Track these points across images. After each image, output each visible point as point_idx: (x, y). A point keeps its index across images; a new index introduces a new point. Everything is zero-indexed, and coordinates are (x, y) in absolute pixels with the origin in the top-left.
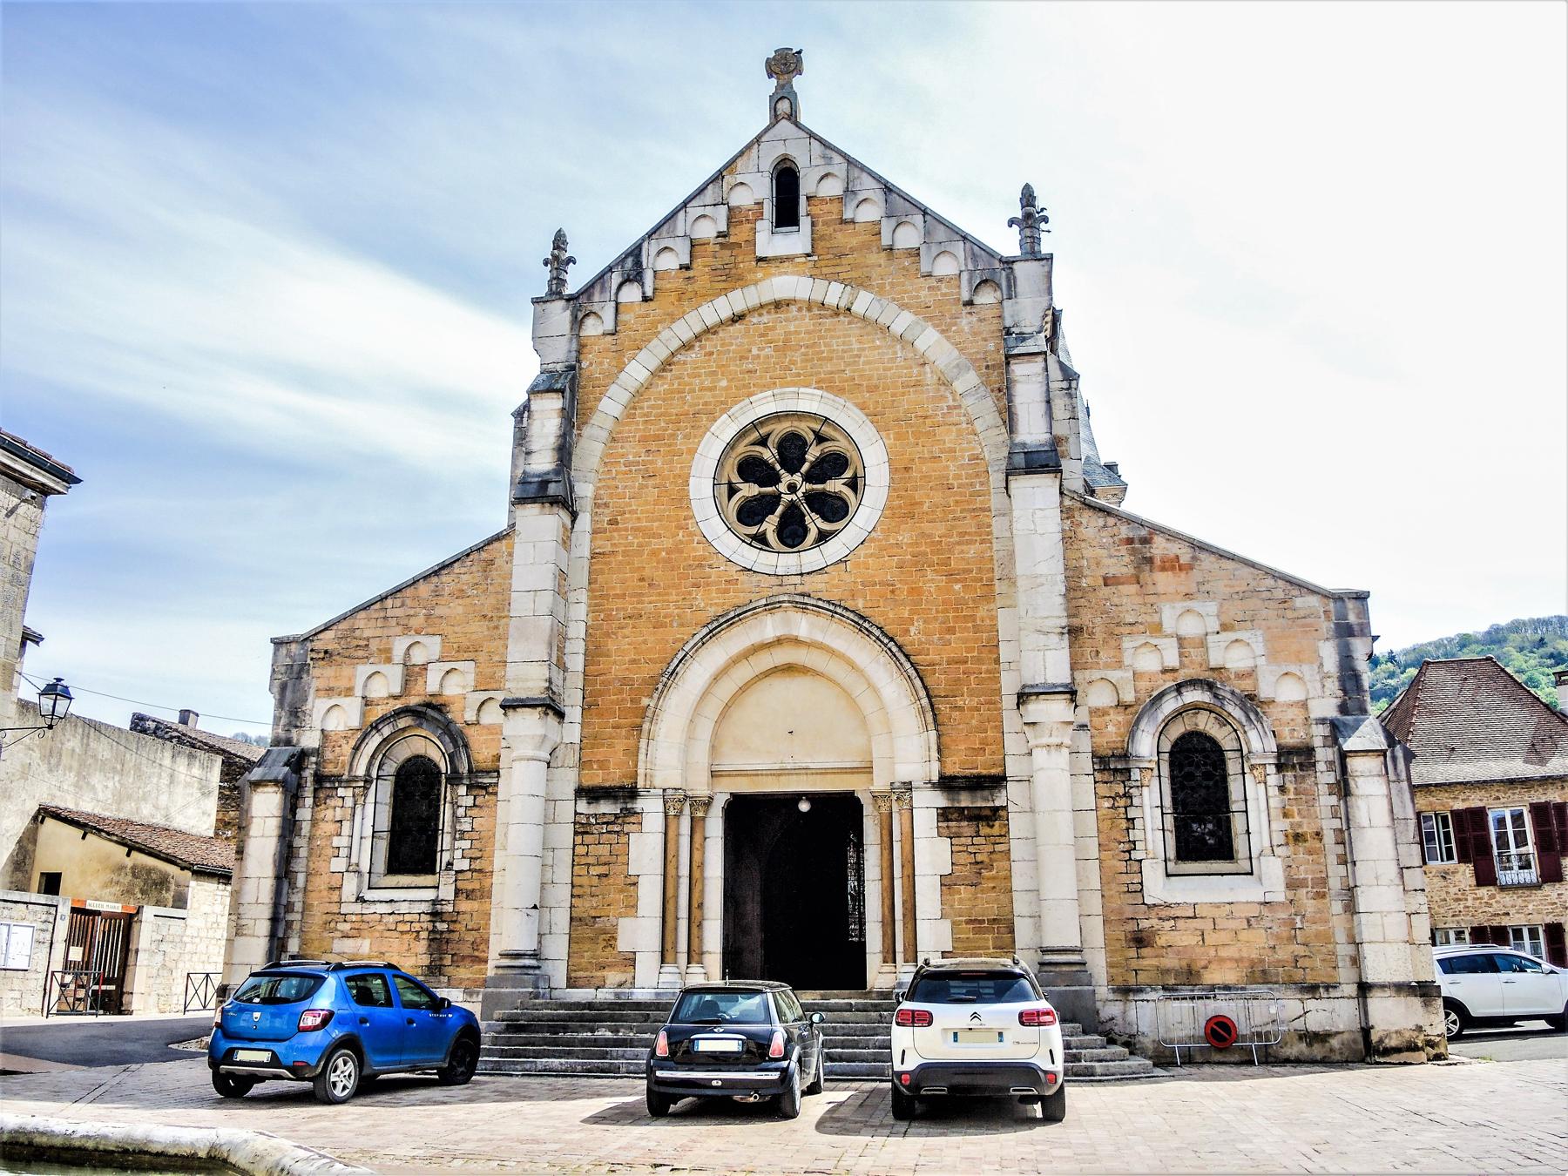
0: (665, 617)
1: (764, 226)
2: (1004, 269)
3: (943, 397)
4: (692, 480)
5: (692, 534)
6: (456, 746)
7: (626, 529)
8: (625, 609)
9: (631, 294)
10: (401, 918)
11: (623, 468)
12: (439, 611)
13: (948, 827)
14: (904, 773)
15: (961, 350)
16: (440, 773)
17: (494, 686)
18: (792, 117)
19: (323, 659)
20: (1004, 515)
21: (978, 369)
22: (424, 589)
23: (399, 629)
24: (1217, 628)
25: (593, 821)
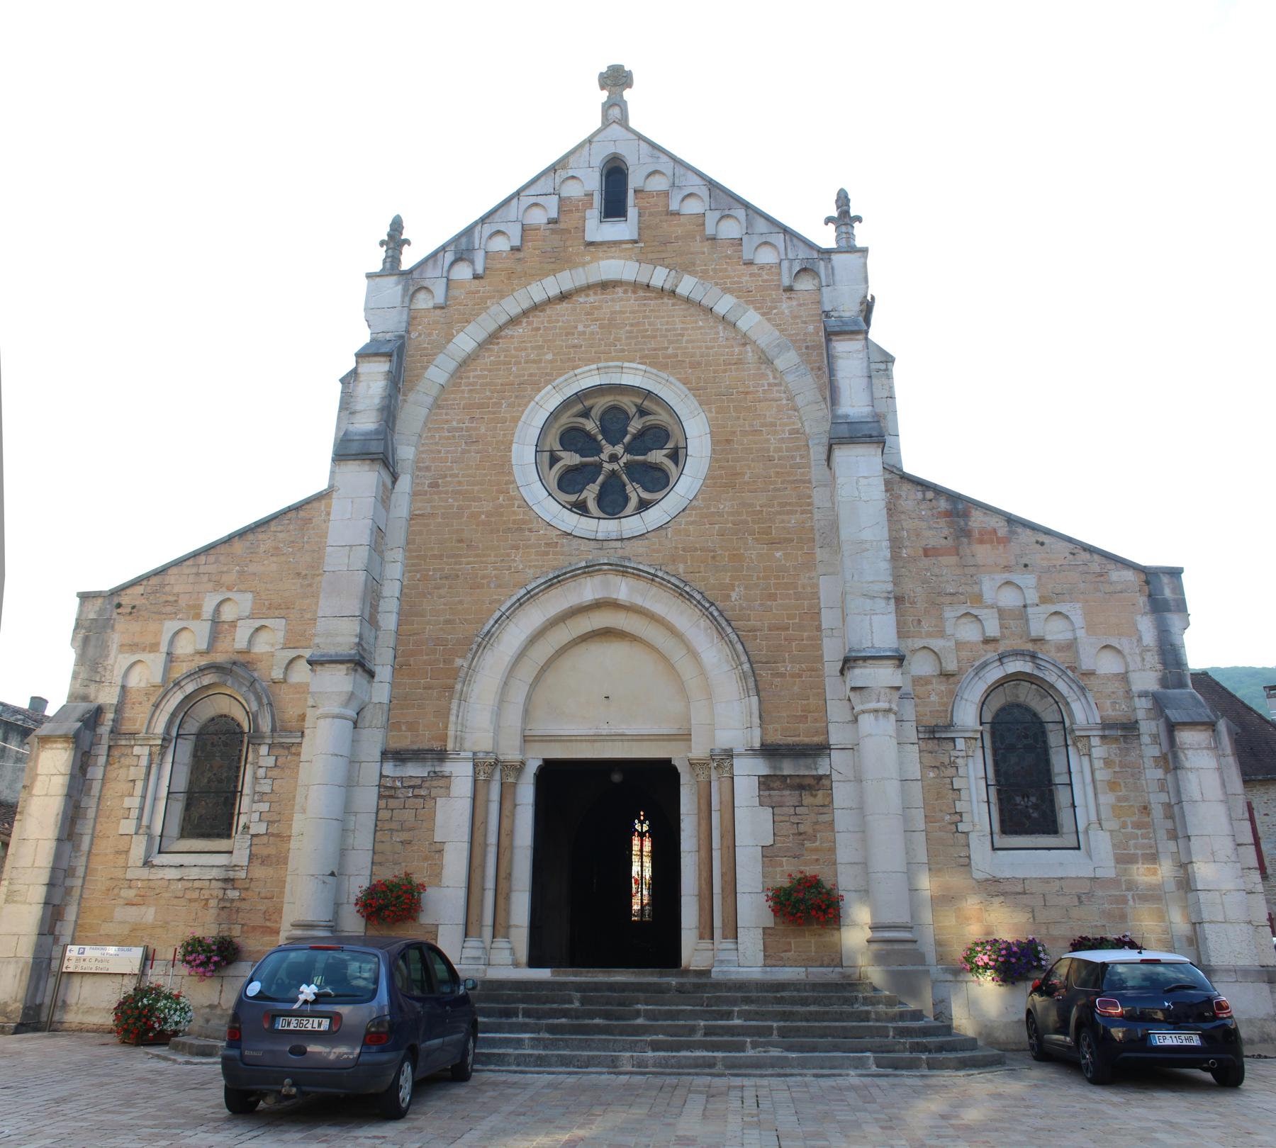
13: (770, 795)
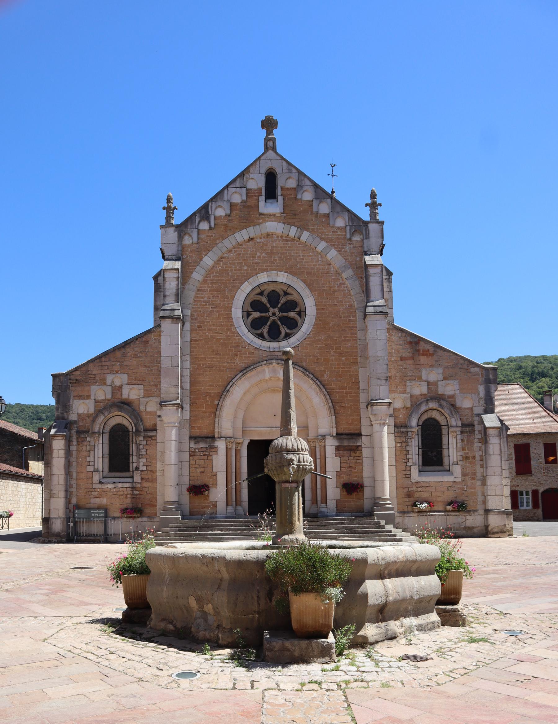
0: (223, 367)
1: (262, 198)
2: (364, 226)
3: (338, 279)
4: (233, 309)
5: (234, 333)
6: (137, 420)
7: (205, 330)
8: (206, 364)
9: (204, 226)
10: (119, 490)
11: (203, 303)
12: (125, 363)
14: (322, 431)
15: (346, 260)
16: (128, 431)
17: (152, 396)
18: (274, 149)
19: (76, 383)
20: (363, 330)
21: (353, 268)
22: (118, 354)
23: (108, 371)
24: (442, 378)
25: (197, 450)
